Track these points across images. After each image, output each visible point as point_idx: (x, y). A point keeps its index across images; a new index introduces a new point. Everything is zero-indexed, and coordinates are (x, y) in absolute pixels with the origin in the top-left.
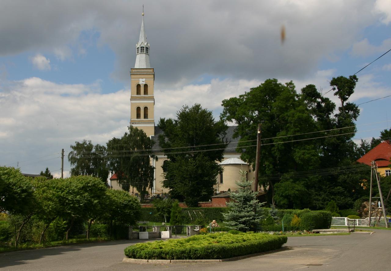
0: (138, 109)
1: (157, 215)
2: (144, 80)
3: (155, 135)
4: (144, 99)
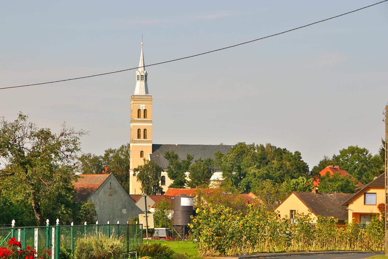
0: (139, 130)
1: (142, 77)
2: (144, 105)
3: (152, 153)
4: (144, 122)
